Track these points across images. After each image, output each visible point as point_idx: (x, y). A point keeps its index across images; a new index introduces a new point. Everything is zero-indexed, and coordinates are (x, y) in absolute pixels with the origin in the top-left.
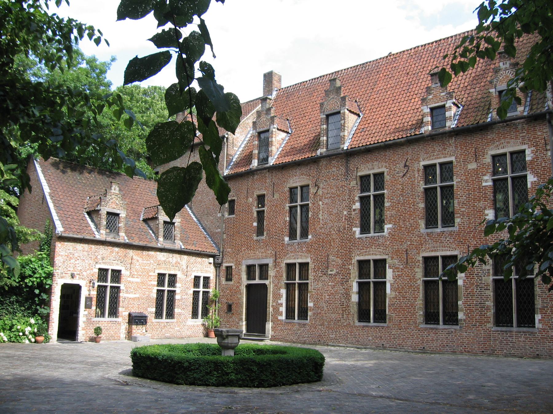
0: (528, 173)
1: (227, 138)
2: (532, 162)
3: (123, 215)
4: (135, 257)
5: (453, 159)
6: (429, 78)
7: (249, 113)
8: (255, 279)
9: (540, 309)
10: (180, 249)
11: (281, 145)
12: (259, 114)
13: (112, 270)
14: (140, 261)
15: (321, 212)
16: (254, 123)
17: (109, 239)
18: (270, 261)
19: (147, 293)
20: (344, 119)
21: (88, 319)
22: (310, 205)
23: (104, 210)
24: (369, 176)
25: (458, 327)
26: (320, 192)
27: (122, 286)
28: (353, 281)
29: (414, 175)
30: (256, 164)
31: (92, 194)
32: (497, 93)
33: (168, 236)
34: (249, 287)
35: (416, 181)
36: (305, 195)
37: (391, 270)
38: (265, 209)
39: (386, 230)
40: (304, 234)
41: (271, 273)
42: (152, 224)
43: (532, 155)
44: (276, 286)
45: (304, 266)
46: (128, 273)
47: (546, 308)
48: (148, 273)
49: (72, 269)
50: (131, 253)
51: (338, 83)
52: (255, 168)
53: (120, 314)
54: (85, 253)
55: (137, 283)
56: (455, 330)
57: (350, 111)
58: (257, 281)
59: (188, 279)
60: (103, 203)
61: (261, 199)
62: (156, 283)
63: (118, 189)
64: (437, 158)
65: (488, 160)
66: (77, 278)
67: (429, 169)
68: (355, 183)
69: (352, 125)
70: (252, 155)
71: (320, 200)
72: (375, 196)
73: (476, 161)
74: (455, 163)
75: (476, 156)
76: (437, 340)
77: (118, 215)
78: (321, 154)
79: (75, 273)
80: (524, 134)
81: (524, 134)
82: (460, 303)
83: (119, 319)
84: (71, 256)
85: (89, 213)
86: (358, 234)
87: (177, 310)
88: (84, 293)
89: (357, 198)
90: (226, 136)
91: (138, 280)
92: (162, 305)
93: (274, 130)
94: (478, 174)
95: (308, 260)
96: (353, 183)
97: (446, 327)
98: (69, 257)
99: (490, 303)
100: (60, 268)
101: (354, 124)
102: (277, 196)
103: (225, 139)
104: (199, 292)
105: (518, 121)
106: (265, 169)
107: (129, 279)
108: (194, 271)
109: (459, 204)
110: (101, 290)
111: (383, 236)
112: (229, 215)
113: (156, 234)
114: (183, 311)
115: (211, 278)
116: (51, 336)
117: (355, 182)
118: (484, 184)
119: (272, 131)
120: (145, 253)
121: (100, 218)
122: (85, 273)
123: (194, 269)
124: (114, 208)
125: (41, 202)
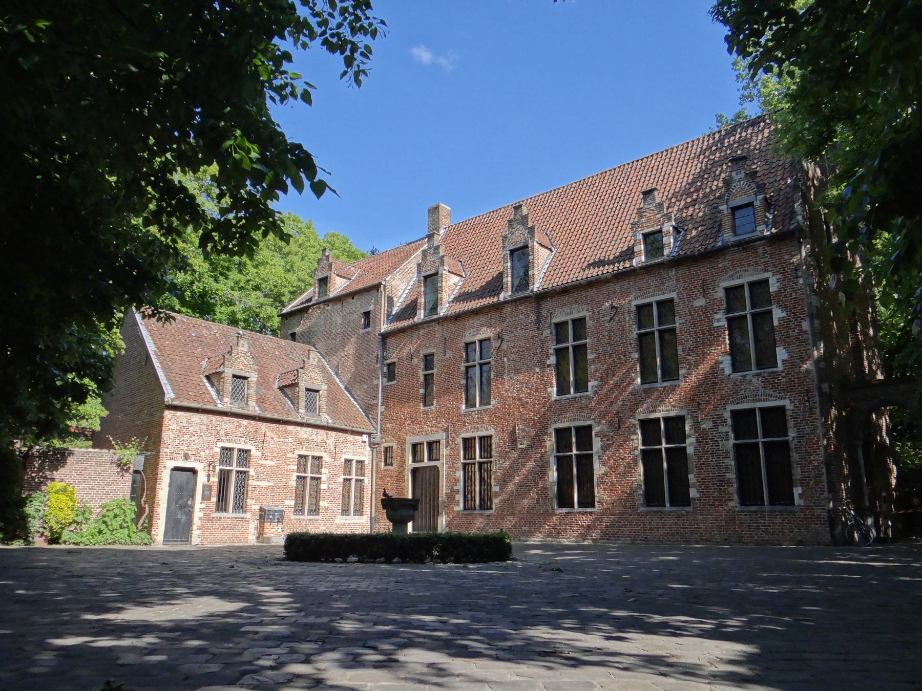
0: (774, 307)
1: (384, 286)
2: (778, 292)
3: (253, 377)
4: (268, 434)
5: (674, 295)
6: (641, 196)
7: (411, 256)
8: (423, 461)
9: (800, 480)
10: (327, 425)
11: (453, 291)
12: (424, 253)
13: (240, 450)
14: (276, 438)
15: (506, 371)
16: (419, 265)
17: (236, 409)
18: (441, 436)
19: (284, 480)
20: (533, 255)
21: (205, 515)
22: (493, 363)
23: (229, 372)
24: (566, 323)
25: (690, 509)
26: (505, 346)
27: (252, 472)
28: (550, 455)
29: (625, 318)
30: (422, 317)
31: (211, 355)
32: (730, 211)
33: (311, 407)
34: (415, 471)
35: (627, 325)
36: (484, 351)
37: (599, 439)
38: (435, 371)
39: (590, 388)
40: (485, 401)
41: (444, 451)
42: (289, 391)
43: (778, 284)
44: (450, 467)
45: (486, 441)
46: (259, 454)
47: (807, 479)
48: (285, 454)
49: (186, 448)
50: (263, 426)
51: (525, 211)
52: (420, 321)
53: (249, 507)
54: (204, 427)
55: (271, 466)
56: (687, 512)
57: (541, 244)
58: (426, 463)
59: (337, 463)
60: (227, 363)
61: (428, 361)
62: (295, 467)
63: (246, 345)
64: (654, 296)
65: (720, 294)
66: (192, 459)
67: (644, 310)
68: (549, 332)
69: (543, 261)
70: (416, 305)
71: (505, 356)
72: (574, 347)
73: (704, 297)
74: (676, 300)
75: (704, 290)
76: (663, 526)
77: (246, 378)
78: (505, 298)
79: (190, 453)
80: (767, 259)
81: (767, 259)
82: (691, 476)
83: (248, 515)
84: (185, 430)
85: (208, 377)
86: (554, 396)
87: (323, 504)
88: (202, 479)
89: (551, 351)
90: (383, 283)
91: (273, 463)
92: (303, 497)
93: (444, 272)
94: (707, 311)
95: (491, 432)
96: (547, 332)
97: (674, 509)
98: (182, 431)
99: (732, 476)
100: (170, 447)
101: (546, 260)
102: (449, 354)
103: (382, 286)
104: (350, 480)
105: (758, 243)
106: (434, 321)
107: (260, 462)
108: (345, 453)
109: (684, 351)
110: (224, 478)
111: (587, 396)
112: (388, 381)
113: (295, 403)
114: (330, 505)
115: (366, 463)
116: (155, 537)
117: (548, 331)
118: (715, 324)
119: (442, 274)
120: (282, 427)
121: (223, 382)
122: (202, 453)
123: (344, 450)
124: (241, 370)
125: (143, 363)
